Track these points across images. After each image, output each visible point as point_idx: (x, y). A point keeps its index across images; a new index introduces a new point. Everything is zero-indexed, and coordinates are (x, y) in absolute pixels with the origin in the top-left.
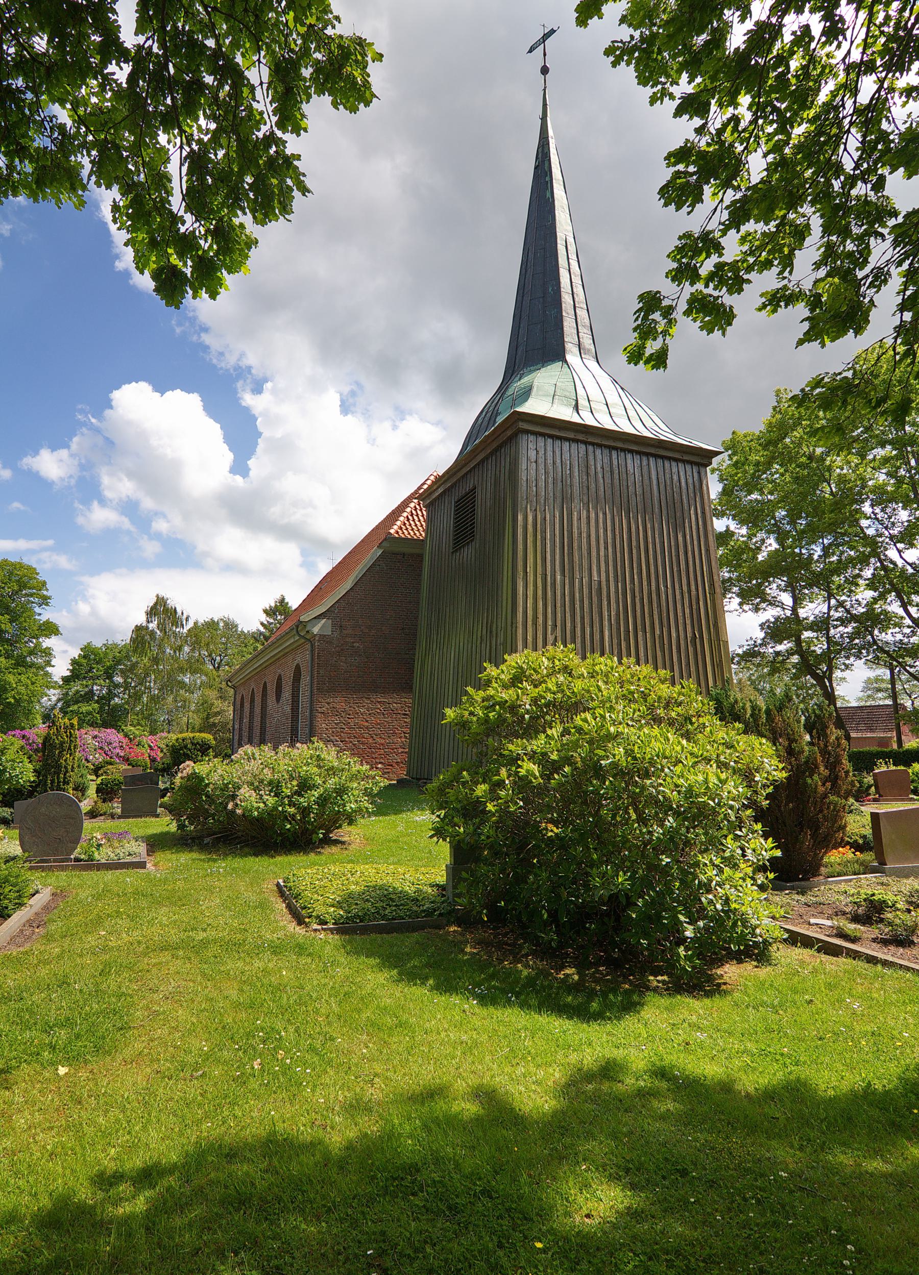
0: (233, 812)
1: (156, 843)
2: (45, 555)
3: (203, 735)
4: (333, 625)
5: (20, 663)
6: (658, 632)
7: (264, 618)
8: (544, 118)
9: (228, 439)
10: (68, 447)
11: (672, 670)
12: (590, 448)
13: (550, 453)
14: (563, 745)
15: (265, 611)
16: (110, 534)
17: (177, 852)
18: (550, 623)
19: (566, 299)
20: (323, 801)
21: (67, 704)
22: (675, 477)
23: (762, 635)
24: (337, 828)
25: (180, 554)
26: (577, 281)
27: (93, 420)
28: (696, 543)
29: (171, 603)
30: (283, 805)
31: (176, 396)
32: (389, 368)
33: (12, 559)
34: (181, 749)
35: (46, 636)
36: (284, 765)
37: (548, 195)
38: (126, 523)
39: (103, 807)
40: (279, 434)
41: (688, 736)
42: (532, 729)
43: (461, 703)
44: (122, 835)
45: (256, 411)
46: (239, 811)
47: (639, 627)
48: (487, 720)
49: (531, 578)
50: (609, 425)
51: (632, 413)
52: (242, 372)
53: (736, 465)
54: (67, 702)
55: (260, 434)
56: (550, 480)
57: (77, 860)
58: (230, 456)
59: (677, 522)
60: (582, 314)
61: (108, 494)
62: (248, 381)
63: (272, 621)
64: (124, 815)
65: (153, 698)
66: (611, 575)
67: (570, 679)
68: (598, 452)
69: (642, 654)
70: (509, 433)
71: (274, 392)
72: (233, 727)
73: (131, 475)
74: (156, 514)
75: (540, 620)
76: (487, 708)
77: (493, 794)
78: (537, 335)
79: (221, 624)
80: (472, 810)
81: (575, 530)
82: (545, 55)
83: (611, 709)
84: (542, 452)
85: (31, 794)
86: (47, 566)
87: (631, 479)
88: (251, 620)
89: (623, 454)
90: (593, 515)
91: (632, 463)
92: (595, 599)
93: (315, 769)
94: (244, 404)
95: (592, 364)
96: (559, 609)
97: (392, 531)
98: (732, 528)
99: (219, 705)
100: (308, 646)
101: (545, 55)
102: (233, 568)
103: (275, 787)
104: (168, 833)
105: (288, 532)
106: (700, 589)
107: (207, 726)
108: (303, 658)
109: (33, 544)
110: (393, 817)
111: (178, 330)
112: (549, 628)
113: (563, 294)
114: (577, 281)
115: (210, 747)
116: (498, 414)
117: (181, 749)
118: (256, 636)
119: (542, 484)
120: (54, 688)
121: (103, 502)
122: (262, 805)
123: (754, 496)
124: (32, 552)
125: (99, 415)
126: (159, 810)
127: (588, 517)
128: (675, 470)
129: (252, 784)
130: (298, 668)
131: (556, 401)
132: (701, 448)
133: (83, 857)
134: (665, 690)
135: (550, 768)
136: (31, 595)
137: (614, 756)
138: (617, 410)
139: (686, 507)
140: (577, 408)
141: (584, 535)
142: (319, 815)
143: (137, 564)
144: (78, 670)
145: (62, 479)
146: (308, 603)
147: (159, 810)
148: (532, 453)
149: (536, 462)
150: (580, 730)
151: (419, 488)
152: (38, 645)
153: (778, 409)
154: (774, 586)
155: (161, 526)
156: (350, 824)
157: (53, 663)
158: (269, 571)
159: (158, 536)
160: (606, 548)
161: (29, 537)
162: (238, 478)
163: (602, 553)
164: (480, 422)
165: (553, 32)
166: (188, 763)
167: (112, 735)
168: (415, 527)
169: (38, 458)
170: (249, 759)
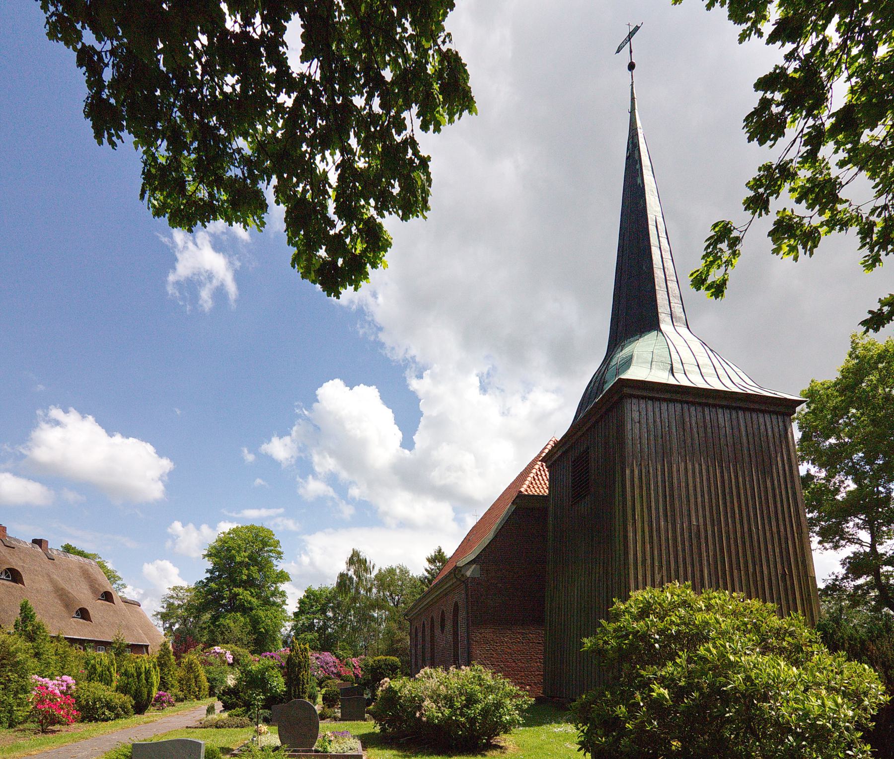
0: (420, 718)
1: (367, 741)
2: (279, 520)
3: (392, 658)
4: (482, 570)
5: (266, 602)
6: (751, 570)
7: (427, 565)
8: (632, 112)
9: (397, 422)
10: (290, 434)
11: (779, 603)
12: (686, 407)
13: (651, 414)
14: (690, 672)
15: (428, 560)
16: (321, 500)
17: (382, 749)
18: (656, 564)
19: (658, 274)
20: (485, 712)
21: (297, 634)
22: (762, 428)
23: (844, 571)
24: (496, 735)
25: (368, 516)
26: (667, 256)
27: (306, 413)
28: (783, 487)
29: (362, 555)
30: (456, 715)
31: (361, 389)
32: (515, 350)
33: (257, 525)
34: (378, 668)
35: (281, 582)
36: (454, 682)
37: (639, 181)
38: (331, 492)
39: (328, 711)
40: (434, 413)
41: (796, 663)
42: (659, 659)
43: (596, 633)
44: (343, 734)
45: (421, 394)
46: (424, 719)
47: (734, 566)
48: (620, 649)
49: (639, 525)
50: (701, 384)
51: (721, 372)
52: (408, 363)
53: (813, 412)
54: (299, 630)
55: (421, 414)
56: (652, 438)
57: (316, 751)
58: (400, 435)
59: (766, 468)
60: (672, 285)
61: (317, 469)
62: (413, 369)
63: (433, 567)
64: (344, 718)
65: (354, 629)
66: (708, 519)
67: (691, 612)
68: (692, 409)
69: (753, 590)
70: (616, 398)
71: (433, 377)
72: (411, 651)
73: (332, 454)
74: (350, 483)
75: (649, 561)
76: (618, 638)
77: (631, 716)
78: (634, 309)
79: (398, 571)
80: (613, 724)
81: (675, 481)
82: (631, 52)
83: (731, 640)
84: (643, 413)
85: (281, 701)
86: (281, 528)
87: (723, 432)
88: (419, 568)
89: (714, 410)
90: (690, 466)
91: (723, 418)
92: (694, 542)
93: (478, 687)
94: (411, 389)
95: (683, 330)
96: (664, 552)
97: (522, 490)
98: (812, 472)
99: (400, 634)
100: (463, 586)
101: (631, 52)
102: (405, 524)
103: (449, 700)
104: (374, 733)
105: (443, 493)
106: (788, 529)
107: (391, 651)
108: (459, 597)
109: (271, 512)
110: (536, 728)
111: (361, 332)
112: (656, 568)
113: (655, 270)
114: (667, 256)
115: (397, 668)
116: (605, 383)
117: (378, 668)
118: (422, 580)
119: (645, 441)
120: (288, 621)
121: (315, 476)
122: (440, 715)
123: (833, 441)
124: (270, 518)
125: (309, 407)
126: (366, 715)
127: (686, 468)
128: (761, 420)
129: (432, 697)
130: (456, 605)
131: (654, 367)
132: (785, 399)
133: (320, 749)
134: (775, 621)
135: (679, 693)
136: (271, 551)
137: (734, 682)
138: (708, 370)
139: (773, 453)
140: (672, 371)
141: (683, 484)
142: (483, 724)
143: (340, 525)
144: (304, 606)
145: (287, 459)
146: (462, 550)
147: (366, 715)
148: (636, 413)
149: (639, 422)
150: (703, 659)
151: (542, 452)
152: (276, 588)
153: (853, 356)
154: (851, 524)
155: (355, 492)
156: (505, 732)
157: (287, 602)
158: (431, 527)
159: (351, 501)
160: (703, 496)
161: (268, 507)
162: (407, 451)
163: (699, 500)
164: (589, 391)
165: (637, 28)
166: (386, 679)
167: (329, 657)
168: (539, 485)
169: (271, 444)
170: (428, 678)
